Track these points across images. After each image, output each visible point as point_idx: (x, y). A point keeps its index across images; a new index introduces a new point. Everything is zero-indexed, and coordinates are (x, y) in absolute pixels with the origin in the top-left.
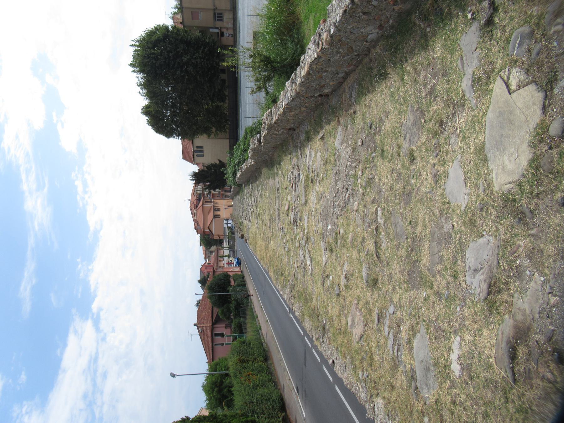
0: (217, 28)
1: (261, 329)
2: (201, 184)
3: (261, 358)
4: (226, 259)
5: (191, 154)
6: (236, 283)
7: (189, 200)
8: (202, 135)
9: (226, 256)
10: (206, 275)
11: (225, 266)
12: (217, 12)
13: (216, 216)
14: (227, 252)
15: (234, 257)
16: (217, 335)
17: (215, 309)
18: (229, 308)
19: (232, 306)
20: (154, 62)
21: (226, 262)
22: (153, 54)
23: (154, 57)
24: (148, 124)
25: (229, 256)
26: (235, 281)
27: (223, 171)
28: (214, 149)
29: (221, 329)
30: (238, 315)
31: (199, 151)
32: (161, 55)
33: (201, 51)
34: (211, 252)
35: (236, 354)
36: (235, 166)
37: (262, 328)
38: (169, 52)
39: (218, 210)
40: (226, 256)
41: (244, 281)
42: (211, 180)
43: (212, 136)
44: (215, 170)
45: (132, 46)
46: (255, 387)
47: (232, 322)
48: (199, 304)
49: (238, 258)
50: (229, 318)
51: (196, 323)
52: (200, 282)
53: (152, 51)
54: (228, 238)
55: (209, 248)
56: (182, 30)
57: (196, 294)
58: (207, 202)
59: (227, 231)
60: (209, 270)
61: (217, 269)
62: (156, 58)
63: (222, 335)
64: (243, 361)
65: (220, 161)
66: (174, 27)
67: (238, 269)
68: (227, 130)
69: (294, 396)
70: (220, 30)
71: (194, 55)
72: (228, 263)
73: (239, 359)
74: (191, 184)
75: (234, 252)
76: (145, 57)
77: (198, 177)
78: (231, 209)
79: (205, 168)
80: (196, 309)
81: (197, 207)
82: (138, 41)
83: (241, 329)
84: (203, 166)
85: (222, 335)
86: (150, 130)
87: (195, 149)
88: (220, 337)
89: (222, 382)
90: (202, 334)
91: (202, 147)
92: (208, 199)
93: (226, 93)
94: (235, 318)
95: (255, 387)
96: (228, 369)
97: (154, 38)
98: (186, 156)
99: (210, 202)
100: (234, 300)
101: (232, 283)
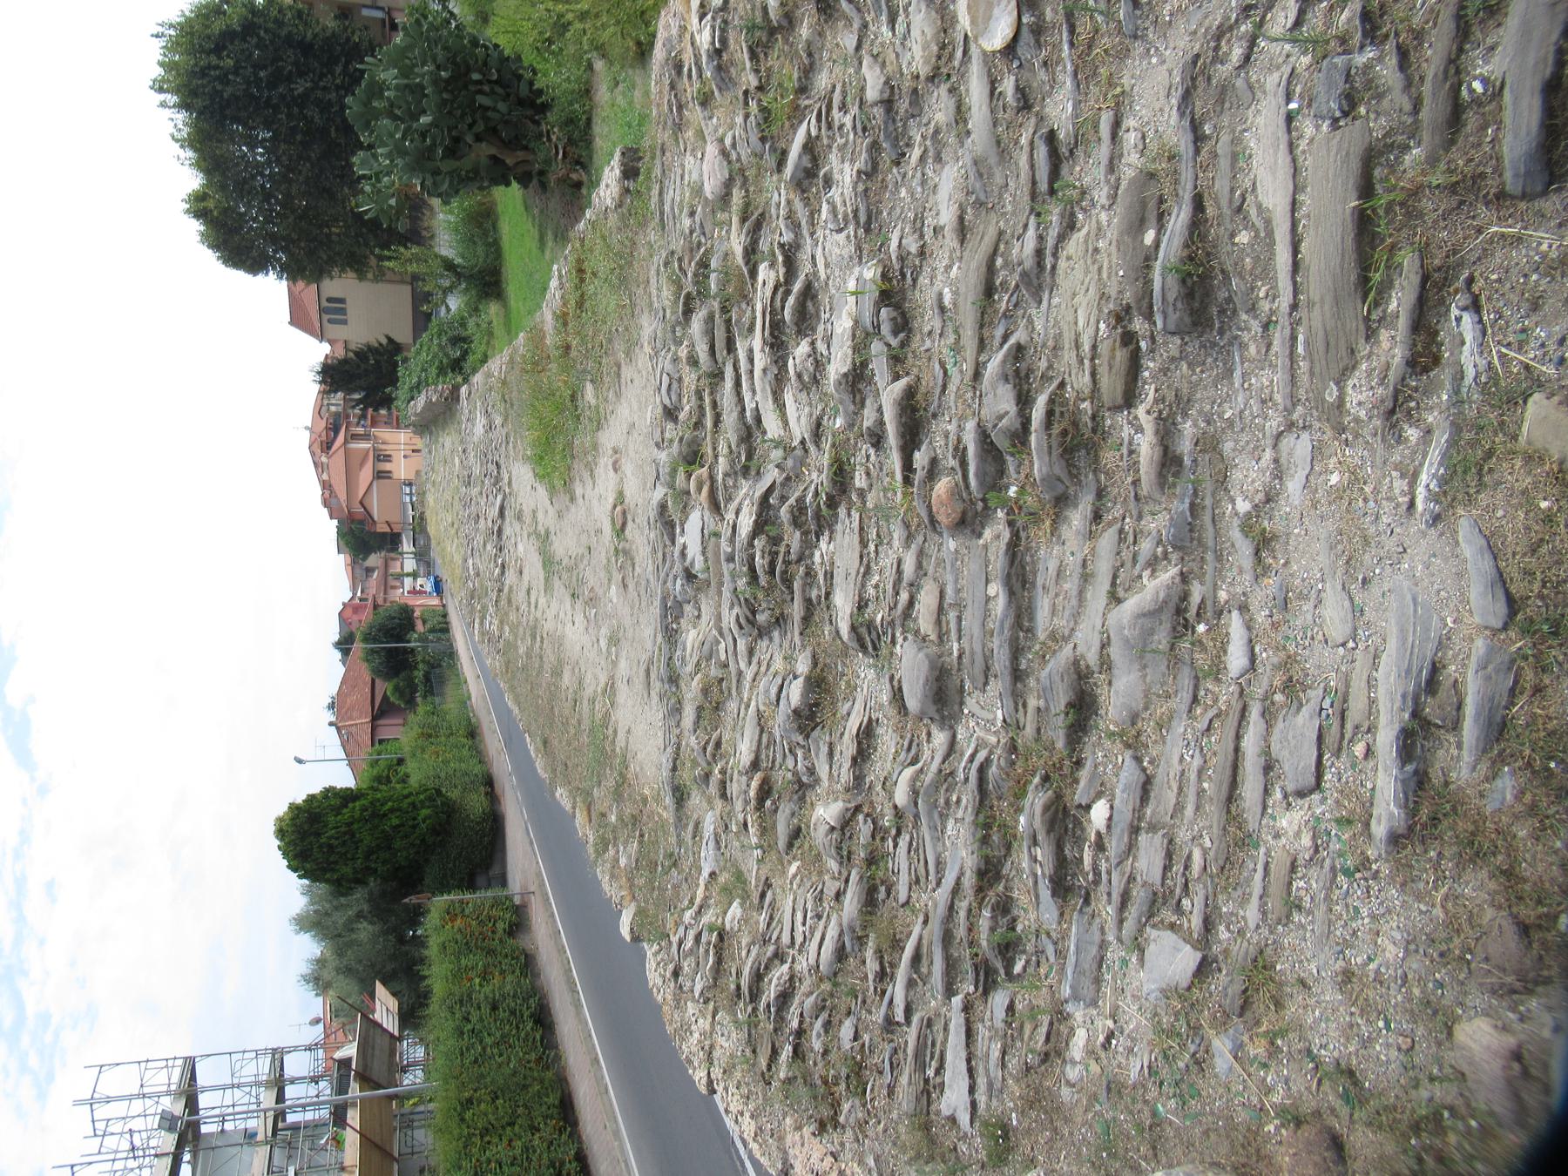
0: (382, 9)
1: (469, 698)
2: (340, 395)
4: (408, 581)
5: (315, 316)
6: (428, 626)
8: (343, 270)
9: (408, 575)
13: (380, 475)
14: (410, 565)
19: (419, 674)
20: (219, 87)
22: (217, 67)
23: (218, 78)
26: (424, 622)
28: (374, 310)
32: (236, 73)
33: (338, 69)
34: (369, 571)
36: (411, 389)
38: (257, 67)
39: (388, 458)
40: (408, 575)
42: (361, 383)
43: (370, 275)
45: (157, 36)
53: (214, 60)
55: (364, 559)
56: (290, 8)
57: (300, 761)
58: (355, 437)
59: (411, 512)
62: (224, 79)
64: (430, 736)
65: (390, 340)
67: (435, 602)
70: (389, 13)
71: (320, 79)
72: (413, 592)
74: (310, 389)
75: (428, 564)
76: (192, 74)
77: (334, 376)
78: (416, 458)
79: (351, 355)
81: (329, 448)
82: (171, 26)
86: (209, 259)
87: (325, 304)
91: (342, 301)
92: (360, 430)
97: (218, 26)
99: (366, 437)
101: (420, 627)
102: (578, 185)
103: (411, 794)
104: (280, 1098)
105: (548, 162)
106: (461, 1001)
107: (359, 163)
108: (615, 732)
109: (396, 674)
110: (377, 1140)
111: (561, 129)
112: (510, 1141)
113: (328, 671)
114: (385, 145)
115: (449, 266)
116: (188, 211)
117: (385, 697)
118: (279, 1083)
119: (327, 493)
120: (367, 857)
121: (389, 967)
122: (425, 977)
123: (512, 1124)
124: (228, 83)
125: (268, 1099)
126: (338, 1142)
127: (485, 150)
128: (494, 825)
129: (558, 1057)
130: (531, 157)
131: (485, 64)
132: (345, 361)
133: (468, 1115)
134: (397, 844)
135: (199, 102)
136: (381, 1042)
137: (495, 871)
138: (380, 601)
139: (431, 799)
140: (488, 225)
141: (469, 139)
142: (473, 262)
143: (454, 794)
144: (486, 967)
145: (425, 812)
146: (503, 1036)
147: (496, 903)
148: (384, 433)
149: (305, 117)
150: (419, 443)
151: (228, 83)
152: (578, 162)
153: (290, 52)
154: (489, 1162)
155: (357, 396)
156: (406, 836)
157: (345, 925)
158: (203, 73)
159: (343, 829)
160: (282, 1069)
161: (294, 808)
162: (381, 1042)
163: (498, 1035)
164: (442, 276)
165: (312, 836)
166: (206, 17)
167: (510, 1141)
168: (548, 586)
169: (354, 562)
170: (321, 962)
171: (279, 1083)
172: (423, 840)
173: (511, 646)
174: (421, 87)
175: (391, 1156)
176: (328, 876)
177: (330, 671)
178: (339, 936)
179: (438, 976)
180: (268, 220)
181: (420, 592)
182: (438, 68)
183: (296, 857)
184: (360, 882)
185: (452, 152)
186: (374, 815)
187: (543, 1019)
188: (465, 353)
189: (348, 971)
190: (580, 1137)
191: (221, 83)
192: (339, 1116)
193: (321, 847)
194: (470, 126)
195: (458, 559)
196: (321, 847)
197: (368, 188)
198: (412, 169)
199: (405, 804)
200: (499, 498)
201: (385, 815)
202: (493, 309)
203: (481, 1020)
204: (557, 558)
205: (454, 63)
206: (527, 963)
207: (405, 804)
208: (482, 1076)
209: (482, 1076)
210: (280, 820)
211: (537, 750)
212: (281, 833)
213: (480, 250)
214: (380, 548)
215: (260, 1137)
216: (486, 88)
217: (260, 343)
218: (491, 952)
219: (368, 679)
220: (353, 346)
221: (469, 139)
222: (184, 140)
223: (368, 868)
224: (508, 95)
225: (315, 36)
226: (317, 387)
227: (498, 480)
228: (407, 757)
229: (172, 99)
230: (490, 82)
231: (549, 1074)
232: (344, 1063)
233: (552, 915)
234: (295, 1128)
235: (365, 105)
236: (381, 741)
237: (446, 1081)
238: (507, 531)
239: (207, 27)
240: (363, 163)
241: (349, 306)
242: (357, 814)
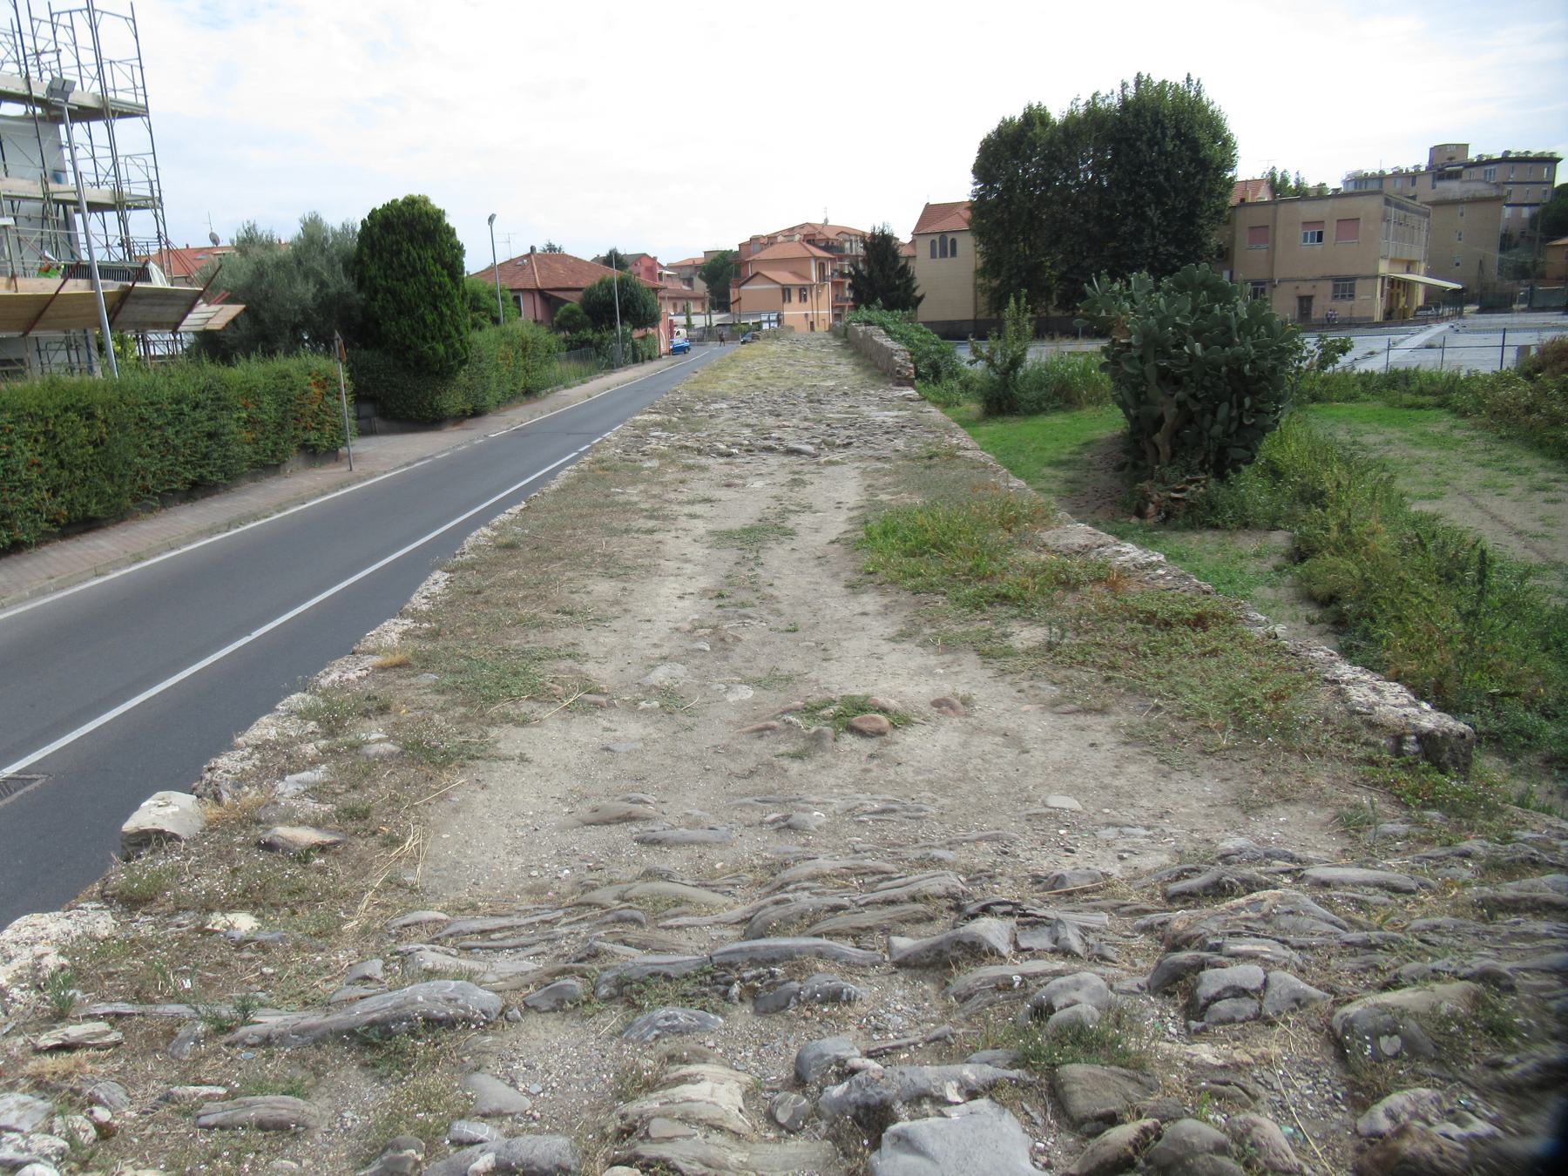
2: (861, 252)
4: (682, 320)
6: (639, 342)
8: (982, 254)
9: (689, 320)
12: (1268, 288)
13: (786, 292)
14: (699, 321)
17: (580, 294)
18: (583, 326)
19: (589, 334)
22: (1164, 135)
23: (1154, 136)
24: (1004, 120)
25: (689, 326)
26: (643, 338)
28: (949, 285)
31: (944, 246)
32: (1160, 153)
33: (1172, 249)
34: (689, 282)
38: (1168, 174)
39: (803, 298)
40: (689, 320)
42: (875, 274)
43: (980, 281)
44: (897, 288)
45: (1188, 79)
53: (1171, 132)
56: (1225, 203)
57: (491, 219)
58: (822, 267)
59: (751, 321)
64: (524, 349)
65: (920, 299)
66: (1230, 184)
67: (664, 348)
72: (672, 325)
74: (865, 223)
75: (700, 340)
77: (880, 245)
78: (806, 328)
79: (903, 262)
81: (809, 242)
84: (908, 258)
86: (989, 126)
87: (949, 237)
91: (954, 253)
92: (829, 272)
97: (1203, 136)
98: (932, 213)
99: (822, 277)
100: (602, 338)
101: (637, 334)
102: (1140, 513)
103: (460, 334)
104: (95, 207)
105: (1163, 481)
106: (219, 399)
107: (1140, 279)
108: (523, 722)
109: (587, 312)
110: (48, 313)
111: (1202, 495)
112: (39, 465)
113: (586, 244)
114: (1168, 306)
115: (1016, 362)
116: (1030, 107)
117: (564, 302)
118: (120, 205)
120: (388, 290)
121: (266, 316)
122: (248, 358)
123: (61, 465)
124: (1151, 147)
125: (103, 194)
126: (46, 271)
127: (1170, 412)
128: (429, 420)
129: (151, 510)
130: (1164, 459)
131: (1259, 411)
132: (896, 257)
133: (72, 415)
134: (405, 322)
135: (1130, 118)
136: (170, 313)
137: (378, 423)
138: (661, 294)
141: (1180, 394)
142: (1021, 387)
143: (462, 378)
144: (262, 422)
145: (441, 349)
146: (175, 447)
147: (339, 430)
148: (827, 293)
149: (1126, 217)
150: (821, 328)
151: (1151, 147)
152: (1169, 515)
153: (1184, 203)
154: (10, 443)
155: (861, 266)
156: (413, 331)
157: (312, 269)
158: (1157, 122)
159: (418, 265)
160: (136, 208)
161: (439, 215)
162: (170, 313)
163: (178, 442)
164: (1004, 355)
165: (407, 238)
166: (1210, 125)
167: (39, 465)
168: (722, 538)
169: (697, 267)
170: (269, 245)
171: (120, 205)
172: (409, 347)
173: (635, 474)
174: (1231, 343)
175: (31, 327)
176: (366, 250)
177: (586, 246)
178: (300, 263)
179: (250, 371)
180: (1025, 183)
181: (672, 332)
182: (1253, 362)
183: (386, 217)
184: (360, 285)
185: (1165, 376)
186: (435, 297)
187: (198, 489)
189: (260, 273)
190: (47, 542)
191: (1149, 140)
192: (78, 270)
193: (398, 242)
194: (1194, 396)
195: (722, 388)
197: (1116, 287)
198: (1146, 335)
200: (810, 448)
201: (436, 308)
202: (973, 407)
203: (195, 422)
204: (764, 556)
205: (1259, 379)
206: (267, 466)
207: (449, 328)
208: (123, 429)
209: (123, 429)
210: (426, 201)
211: (502, 528)
212: (411, 202)
213: (1034, 394)
214: (712, 292)
215: (53, 186)
216: (1234, 413)
217: (908, 174)
218: (280, 427)
219: (582, 284)
221: (1180, 394)
222: (1095, 104)
223: (376, 292)
224: (1229, 436)
225: (1201, 227)
227: (832, 446)
228: (502, 327)
229: (1131, 92)
230: (1241, 416)
231: (128, 502)
232: (143, 274)
233: (324, 494)
234: (68, 223)
235: (1202, 284)
236: (517, 299)
237: (120, 386)
238: (773, 460)
239: (1201, 126)
240: (1142, 281)
241: (948, 260)
242: (435, 279)
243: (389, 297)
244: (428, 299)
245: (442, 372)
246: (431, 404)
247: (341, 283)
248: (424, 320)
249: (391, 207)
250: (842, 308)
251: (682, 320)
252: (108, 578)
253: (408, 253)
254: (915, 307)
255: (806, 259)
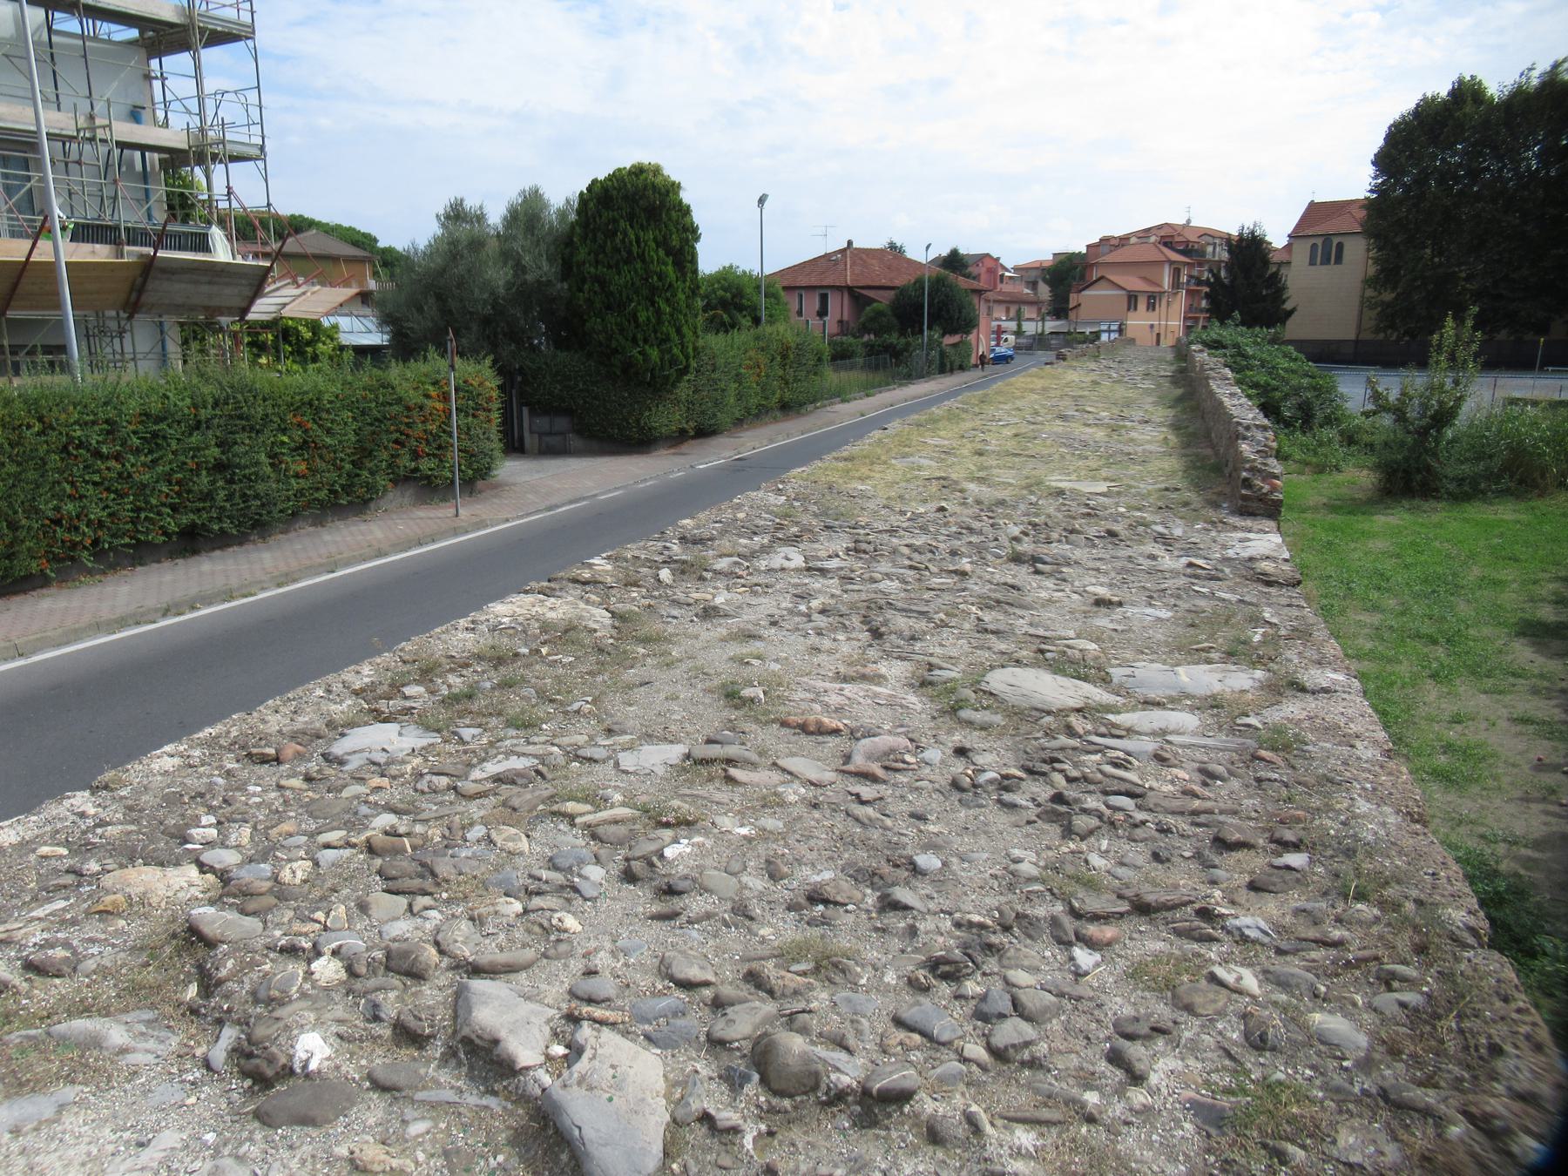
1: (843, 401)
2: (1225, 256)
3: (788, 395)
4: (1013, 325)
6: (948, 350)
7: (1189, 221)
8: (1376, 261)
9: (1019, 326)
10: (972, 270)
11: (995, 324)
13: (1132, 299)
14: (1030, 328)
15: (1017, 348)
16: (824, 298)
19: (893, 338)
21: (1005, 325)
25: (1019, 333)
26: (954, 345)
27: (1233, 319)
28: (1327, 299)
29: (838, 308)
30: (871, 350)
34: (1033, 285)
35: (798, 340)
36: (1236, 346)
37: (846, 406)
39: (1151, 306)
40: (1019, 326)
41: (952, 371)
42: (1238, 282)
43: (1370, 293)
46: (738, 378)
47: (855, 337)
48: (894, 250)
49: (1011, 357)
50: (864, 329)
51: (855, 245)
52: (954, 253)
54: (1069, 333)
55: (1045, 280)
57: (762, 201)
58: (1176, 273)
59: (1088, 331)
60: (983, 277)
61: (988, 301)
63: (822, 312)
64: (784, 357)
65: (1290, 313)
68: (1381, 336)
69: (727, 454)
72: (999, 332)
73: (788, 348)
75: (1029, 348)
77: (1249, 249)
80: (878, 242)
81: (1165, 244)
83: (841, 356)
84: (1280, 264)
85: (822, 312)
87: (1335, 241)
88: (817, 306)
89: (741, 308)
90: (826, 262)
91: (1339, 260)
93: (1502, 335)
94: (866, 345)
95: (738, 378)
96: (771, 323)
98: (1316, 213)
99: (1176, 284)
101: (949, 340)
115: (1443, 417)
117: (871, 301)
119: (1116, 242)
132: (1266, 262)
134: (612, 319)
136: (230, 294)
137: (575, 441)
139: (673, 362)
140: (1506, 482)
143: (683, 390)
145: (654, 354)
148: (1180, 302)
150: (1167, 342)
155: (1223, 274)
156: (622, 331)
159: (635, 249)
165: (635, 212)
176: (578, 229)
186: (653, 290)
188: (1288, 424)
193: (615, 221)
196: (615, 221)
199: (666, 328)
201: (653, 303)
202: (1359, 476)
206: (347, 499)
210: (657, 170)
212: (638, 171)
219: (897, 283)
220: (1283, 271)
223: (584, 281)
226: (1235, 233)
228: (766, 329)
241: (1332, 269)
242: (655, 267)
243: (597, 287)
244: (645, 292)
245: (657, 384)
246: (638, 421)
247: (541, 268)
248: (635, 316)
249: (617, 177)
250: (1196, 319)
251: (1013, 325)
252: (29, 661)
253: (625, 234)
254: (1283, 322)
255: (1161, 263)
